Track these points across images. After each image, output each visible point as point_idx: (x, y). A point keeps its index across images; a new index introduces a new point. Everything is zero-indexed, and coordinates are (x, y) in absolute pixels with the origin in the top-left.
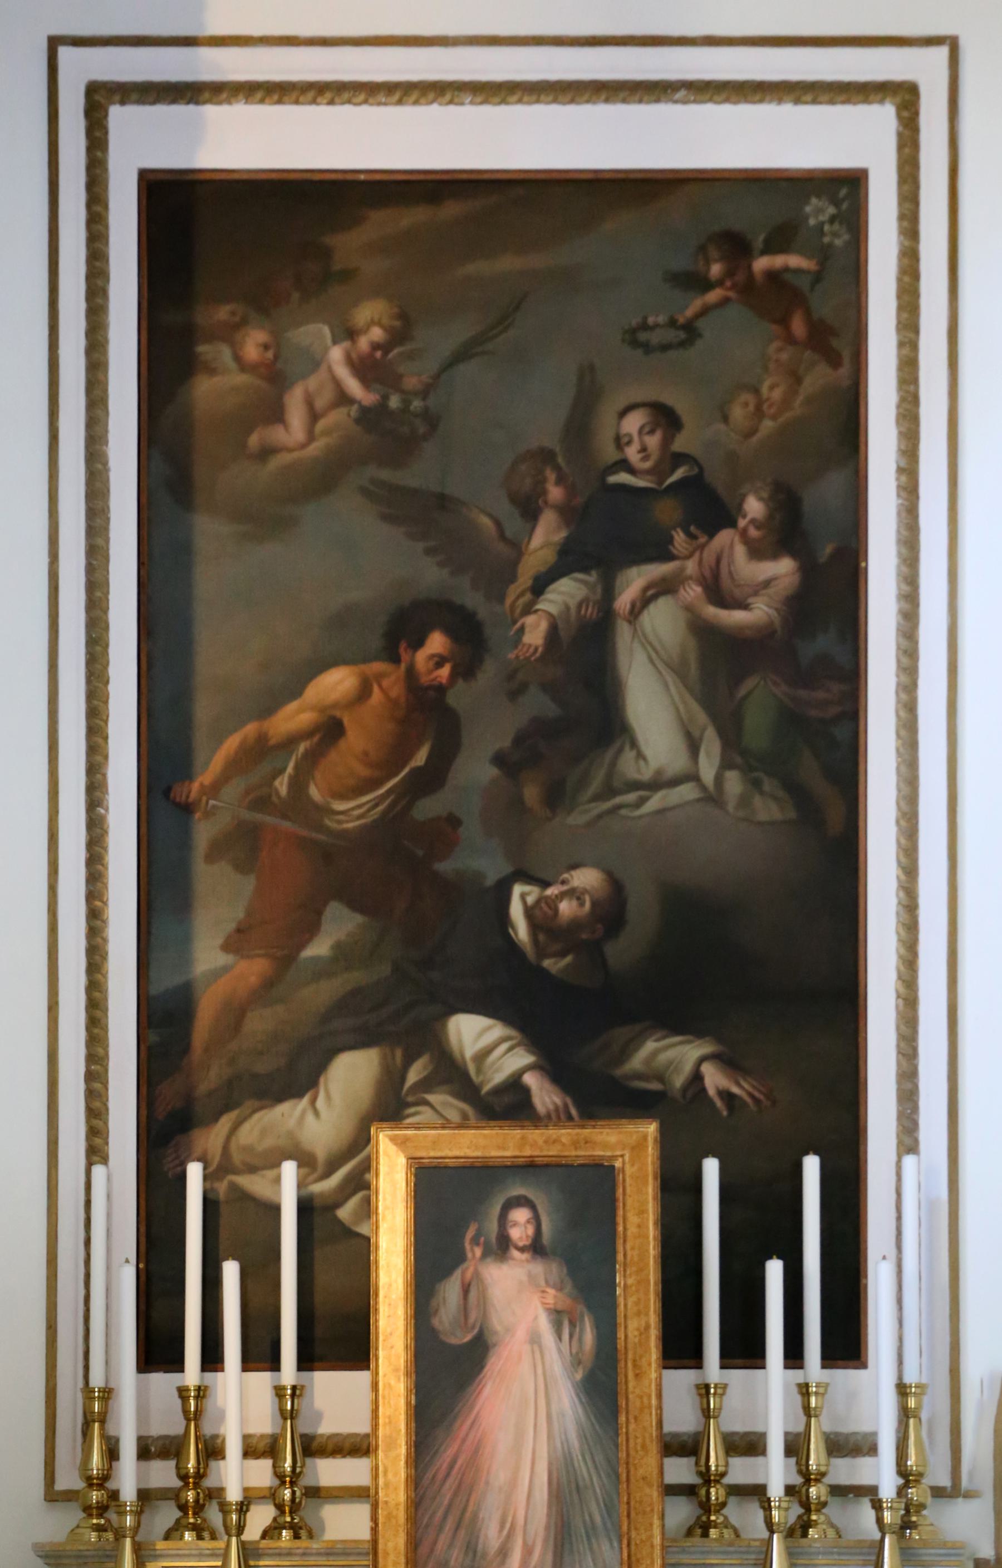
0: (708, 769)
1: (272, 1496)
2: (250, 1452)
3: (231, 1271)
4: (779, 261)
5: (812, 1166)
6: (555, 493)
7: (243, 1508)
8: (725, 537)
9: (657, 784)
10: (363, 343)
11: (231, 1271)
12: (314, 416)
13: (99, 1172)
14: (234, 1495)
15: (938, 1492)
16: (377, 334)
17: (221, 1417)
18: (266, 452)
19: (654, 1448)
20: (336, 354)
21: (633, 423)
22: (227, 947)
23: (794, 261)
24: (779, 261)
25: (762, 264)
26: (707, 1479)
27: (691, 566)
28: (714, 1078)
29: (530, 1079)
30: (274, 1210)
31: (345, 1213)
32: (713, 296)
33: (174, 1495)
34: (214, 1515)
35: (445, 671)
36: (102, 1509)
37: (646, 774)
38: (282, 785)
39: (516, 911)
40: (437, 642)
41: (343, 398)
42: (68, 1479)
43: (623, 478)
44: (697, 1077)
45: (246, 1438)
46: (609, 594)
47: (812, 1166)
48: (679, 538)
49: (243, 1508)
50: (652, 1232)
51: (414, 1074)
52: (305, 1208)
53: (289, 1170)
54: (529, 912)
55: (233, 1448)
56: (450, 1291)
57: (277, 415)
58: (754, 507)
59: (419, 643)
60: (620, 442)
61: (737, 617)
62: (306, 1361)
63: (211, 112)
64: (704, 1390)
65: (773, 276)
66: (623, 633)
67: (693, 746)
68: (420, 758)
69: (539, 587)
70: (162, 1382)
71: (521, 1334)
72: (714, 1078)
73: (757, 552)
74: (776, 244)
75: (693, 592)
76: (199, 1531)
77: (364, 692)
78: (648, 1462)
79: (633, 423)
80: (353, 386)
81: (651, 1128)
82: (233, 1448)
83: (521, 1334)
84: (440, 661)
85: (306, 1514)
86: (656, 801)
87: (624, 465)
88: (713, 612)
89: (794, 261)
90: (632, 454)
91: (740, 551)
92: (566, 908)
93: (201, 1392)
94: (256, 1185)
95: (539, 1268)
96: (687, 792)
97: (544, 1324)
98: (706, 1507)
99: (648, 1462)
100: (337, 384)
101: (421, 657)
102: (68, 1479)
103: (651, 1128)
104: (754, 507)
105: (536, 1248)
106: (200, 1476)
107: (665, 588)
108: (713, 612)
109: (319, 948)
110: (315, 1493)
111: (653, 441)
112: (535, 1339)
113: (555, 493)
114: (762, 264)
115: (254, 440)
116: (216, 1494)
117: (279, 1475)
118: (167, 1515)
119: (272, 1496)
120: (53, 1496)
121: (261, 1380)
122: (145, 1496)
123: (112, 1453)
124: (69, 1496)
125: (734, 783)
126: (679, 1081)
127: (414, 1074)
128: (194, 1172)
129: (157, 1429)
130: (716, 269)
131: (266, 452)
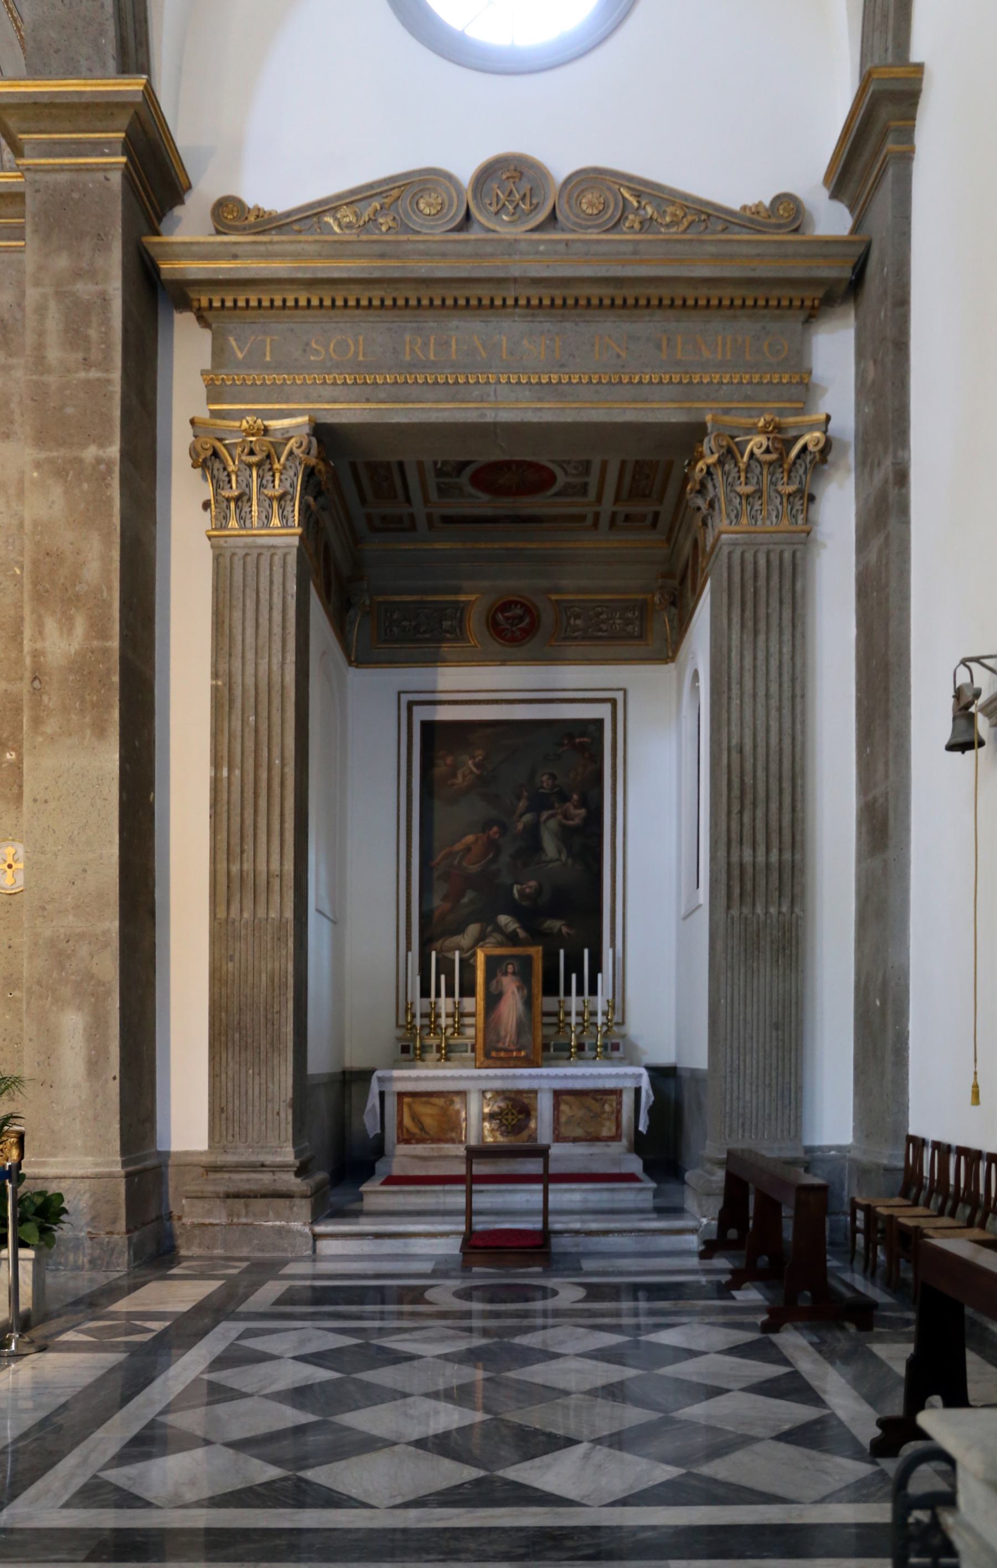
0: (563, 858)
1: (453, 1026)
2: (448, 1016)
3: (443, 977)
4: (582, 740)
5: (586, 952)
6: (525, 794)
7: (446, 1029)
8: (568, 804)
9: (551, 861)
10: (477, 760)
11: (443, 977)
12: (464, 777)
13: (410, 954)
14: (443, 1026)
15: (617, 1024)
16: (480, 757)
17: (440, 1008)
18: (453, 785)
19: (540, 1016)
20: (470, 762)
21: (545, 778)
22: (442, 900)
23: (586, 740)
24: (582, 740)
25: (577, 740)
26: (560, 1021)
27: (559, 811)
28: (564, 930)
29: (519, 930)
30: (453, 961)
31: (471, 961)
32: (565, 748)
33: (429, 1026)
34: (439, 1031)
35: (497, 836)
36: (411, 1029)
37: (548, 859)
38: (456, 862)
39: (515, 891)
40: (495, 829)
41: (472, 772)
42: (402, 1022)
43: (543, 790)
44: (560, 930)
45: (23, 202)
46: (539, 817)
47: (586, 952)
48: (556, 805)
49: (446, 1029)
50: (540, 970)
51: (489, 929)
52: (461, 960)
53: (457, 953)
54: (519, 892)
55: (443, 1015)
56: (494, 983)
57: (455, 776)
58: (575, 797)
59: (490, 829)
60: (542, 782)
61: (571, 823)
62: (461, 995)
63: (439, 707)
64: (559, 1002)
65: (580, 743)
66: (542, 828)
67: (560, 852)
68: (491, 856)
69: (521, 816)
70: (426, 1000)
71: (510, 991)
72: (564, 930)
73: (576, 807)
74: (582, 735)
75: (560, 817)
76: (435, 1034)
77: (476, 841)
78: (538, 1018)
79: (545, 778)
80: (474, 769)
81: (540, 948)
82: (443, 1015)
83: (510, 991)
84: (496, 833)
85: (462, 1029)
86: (551, 865)
87: (543, 788)
88: (565, 821)
89: (586, 740)
90: (545, 785)
91: (572, 808)
92: (528, 890)
93: (435, 1003)
94: (449, 955)
95: (514, 978)
96: (558, 863)
97: (515, 990)
98: (559, 1028)
99: (538, 1018)
100: (470, 769)
101: (491, 833)
102: (402, 1022)
103: (540, 948)
104: (575, 797)
105: (514, 973)
106: (435, 1021)
107: (553, 816)
108: (565, 821)
109: (465, 900)
110: (464, 1025)
111: (550, 782)
112: (513, 993)
113: (525, 794)
114: (577, 740)
115: (449, 782)
116: (439, 1026)
117: (454, 1021)
118: (426, 1031)
119: (453, 1026)
120: (398, 1026)
121: (450, 1000)
122: (422, 1027)
123: (414, 1016)
124: (402, 1026)
125: (570, 861)
126: (556, 930)
127: (489, 929)
128: (434, 954)
129: (424, 1011)
130: (566, 742)
131: (453, 785)
